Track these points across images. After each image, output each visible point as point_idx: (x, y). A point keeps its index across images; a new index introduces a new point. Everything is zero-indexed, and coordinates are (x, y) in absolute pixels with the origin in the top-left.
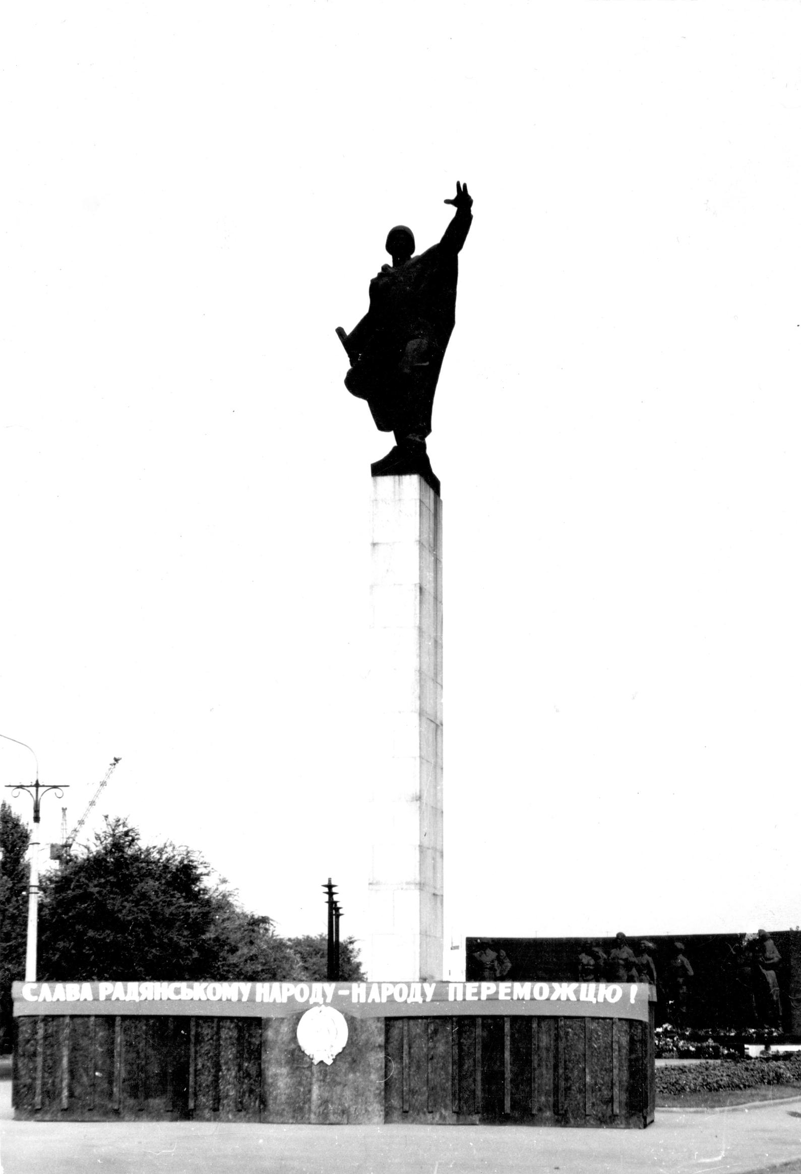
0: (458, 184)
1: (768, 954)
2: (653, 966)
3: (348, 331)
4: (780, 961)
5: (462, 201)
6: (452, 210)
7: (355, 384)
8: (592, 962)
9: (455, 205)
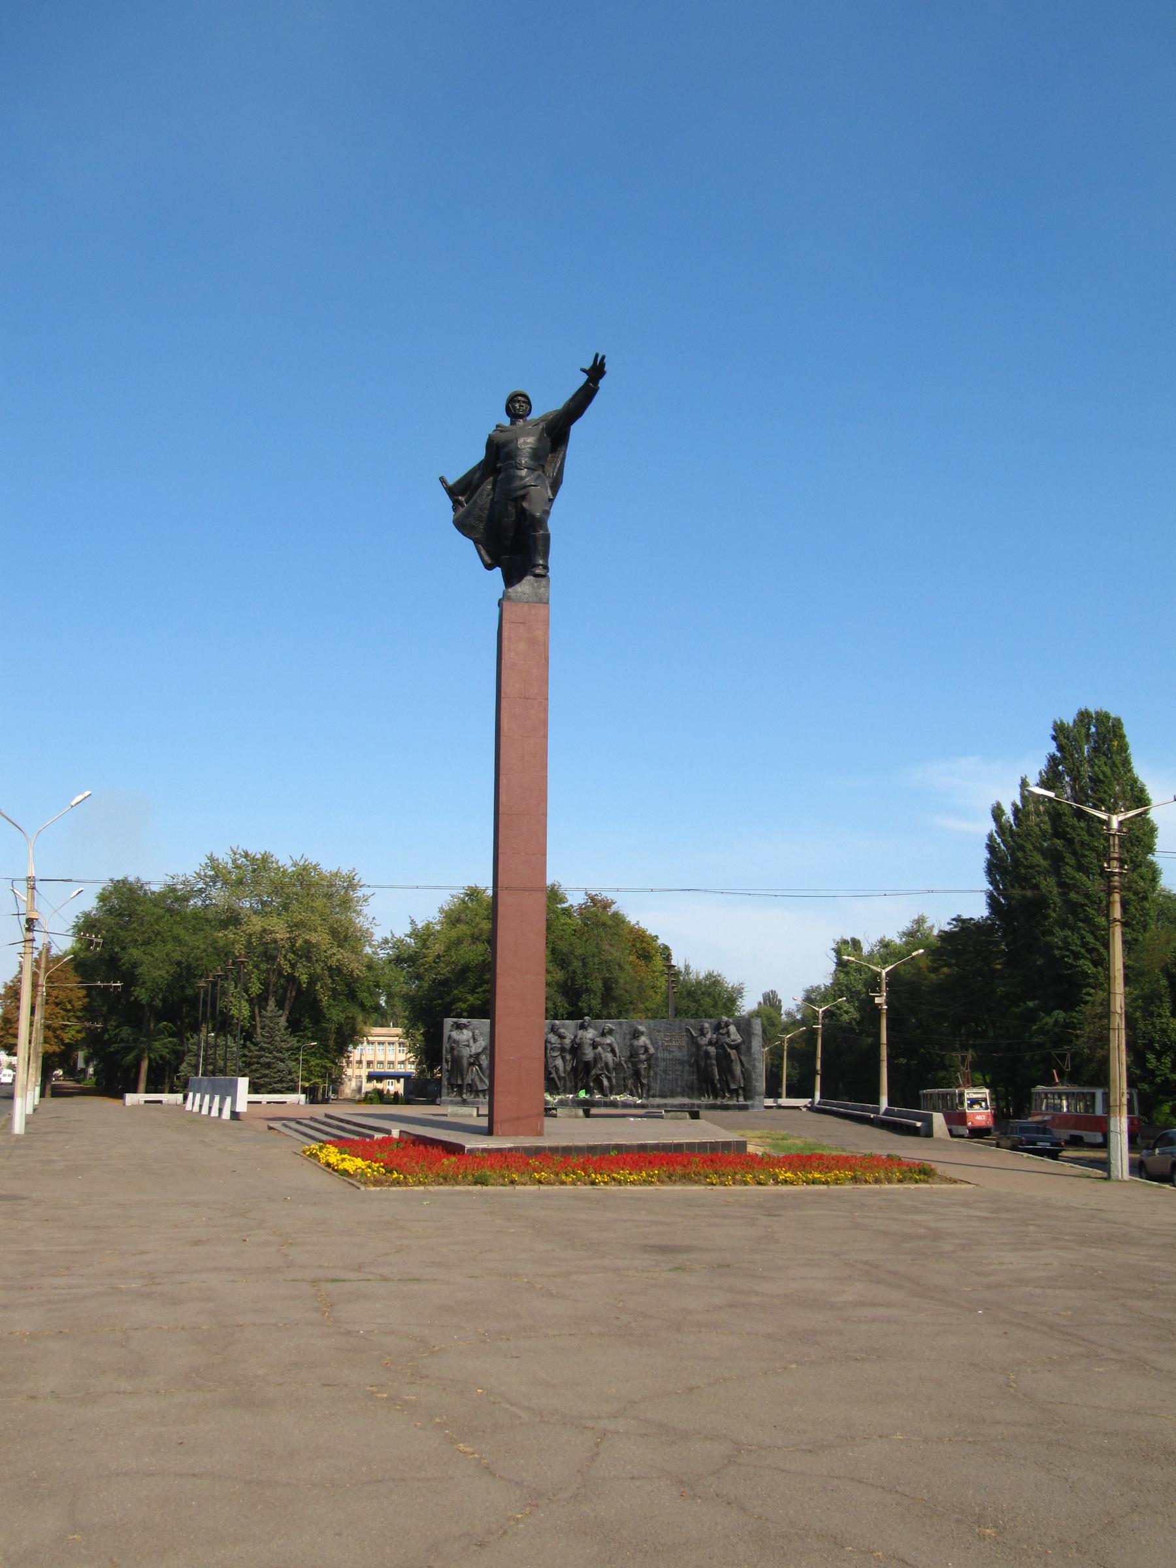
0: (597, 356)
1: (733, 1037)
2: (615, 1045)
3: (451, 481)
4: (743, 1042)
5: (596, 372)
6: (585, 377)
7: (462, 525)
8: (559, 1041)
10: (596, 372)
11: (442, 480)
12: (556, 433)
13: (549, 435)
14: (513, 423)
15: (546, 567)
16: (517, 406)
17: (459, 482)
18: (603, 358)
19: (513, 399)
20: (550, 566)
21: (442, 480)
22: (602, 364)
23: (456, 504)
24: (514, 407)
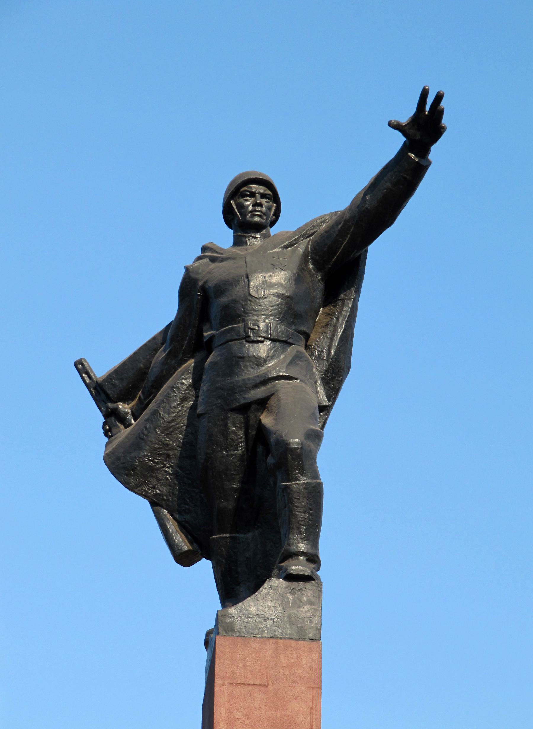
0: (424, 94)
3: (100, 371)
5: (425, 127)
6: (398, 140)
7: (125, 467)
9: (405, 134)
10: (425, 127)
11: (81, 367)
12: (337, 262)
13: (319, 266)
14: (238, 242)
15: (313, 559)
16: (248, 205)
17: (119, 372)
18: (439, 98)
19: (238, 190)
20: (322, 555)
21: (81, 367)
22: (437, 112)
23: (112, 419)
24: (241, 207)
